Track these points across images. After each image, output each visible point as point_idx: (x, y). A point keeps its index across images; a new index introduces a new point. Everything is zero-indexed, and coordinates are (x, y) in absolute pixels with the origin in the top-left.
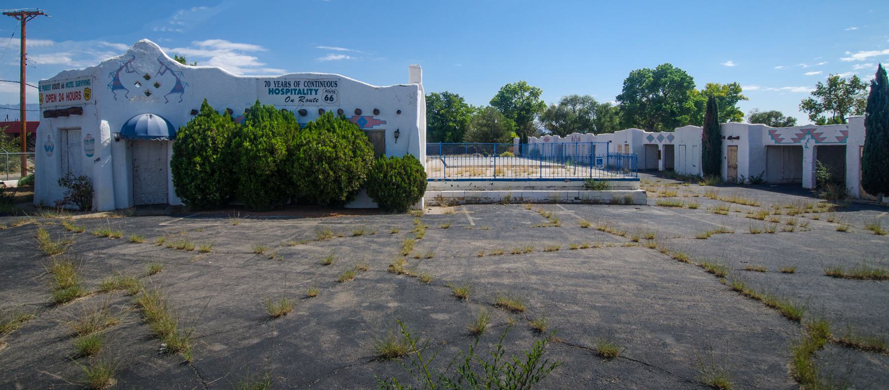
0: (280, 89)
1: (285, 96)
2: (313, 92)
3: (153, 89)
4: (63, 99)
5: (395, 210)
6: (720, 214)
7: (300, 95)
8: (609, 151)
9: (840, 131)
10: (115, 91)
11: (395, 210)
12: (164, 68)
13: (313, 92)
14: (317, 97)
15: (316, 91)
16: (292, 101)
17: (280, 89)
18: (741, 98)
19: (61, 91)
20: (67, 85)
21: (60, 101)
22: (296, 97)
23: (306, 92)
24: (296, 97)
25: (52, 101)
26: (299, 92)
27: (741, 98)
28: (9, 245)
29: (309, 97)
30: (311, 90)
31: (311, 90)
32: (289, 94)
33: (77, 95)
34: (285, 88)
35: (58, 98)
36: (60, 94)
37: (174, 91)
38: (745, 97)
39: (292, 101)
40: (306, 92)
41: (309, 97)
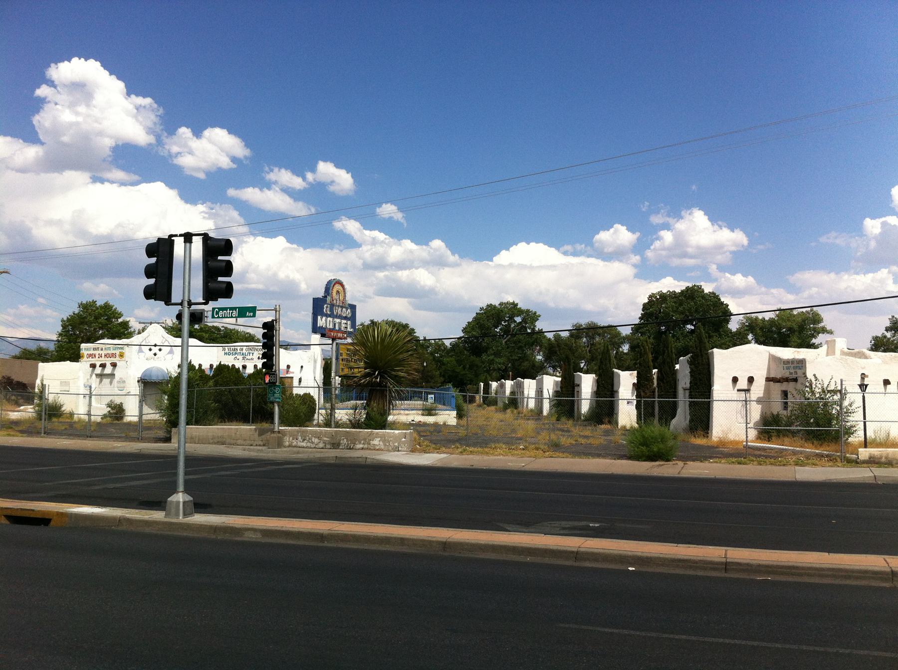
0: (231, 352)
1: (234, 356)
2: (251, 354)
3: (158, 352)
4: (101, 357)
5: (31, 117)
6: (552, 457)
7: (243, 356)
8: (868, 434)
9: (111, 385)
10: (139, 354)
11: (31, 117)
12: (164, 340)
13: (251, 354)
14: (253, 357)
15: (253, 354)
16: (238, 359)
17: (231, 352)
18: (824, 330)
19: (100, 352)
20: (105, 349)
21: (99, 358)
22: (240, 357)
23: (246, 354)
24: (240, 357)
25: (92, 358)
26: (243, 354)
27: (824, 330)
28: (63, 466)
29: (248, 357)
30: (250, 353)
31: (250, 353)
32: (236, 355)
33: (113, 355)
34: (234, 352)
35: (97, 356)
36: (99, 354)
37: (169, 353)
38: (828, 328)
39: (238, 359)
40: (246, 354)
41: (248, 357)
